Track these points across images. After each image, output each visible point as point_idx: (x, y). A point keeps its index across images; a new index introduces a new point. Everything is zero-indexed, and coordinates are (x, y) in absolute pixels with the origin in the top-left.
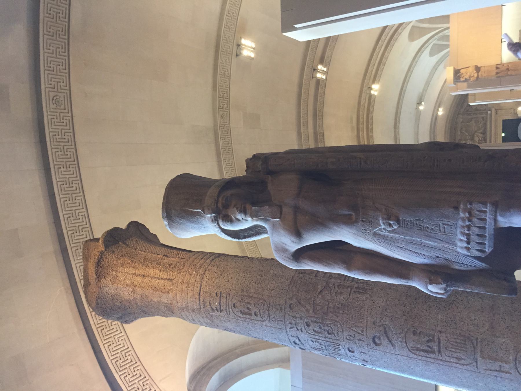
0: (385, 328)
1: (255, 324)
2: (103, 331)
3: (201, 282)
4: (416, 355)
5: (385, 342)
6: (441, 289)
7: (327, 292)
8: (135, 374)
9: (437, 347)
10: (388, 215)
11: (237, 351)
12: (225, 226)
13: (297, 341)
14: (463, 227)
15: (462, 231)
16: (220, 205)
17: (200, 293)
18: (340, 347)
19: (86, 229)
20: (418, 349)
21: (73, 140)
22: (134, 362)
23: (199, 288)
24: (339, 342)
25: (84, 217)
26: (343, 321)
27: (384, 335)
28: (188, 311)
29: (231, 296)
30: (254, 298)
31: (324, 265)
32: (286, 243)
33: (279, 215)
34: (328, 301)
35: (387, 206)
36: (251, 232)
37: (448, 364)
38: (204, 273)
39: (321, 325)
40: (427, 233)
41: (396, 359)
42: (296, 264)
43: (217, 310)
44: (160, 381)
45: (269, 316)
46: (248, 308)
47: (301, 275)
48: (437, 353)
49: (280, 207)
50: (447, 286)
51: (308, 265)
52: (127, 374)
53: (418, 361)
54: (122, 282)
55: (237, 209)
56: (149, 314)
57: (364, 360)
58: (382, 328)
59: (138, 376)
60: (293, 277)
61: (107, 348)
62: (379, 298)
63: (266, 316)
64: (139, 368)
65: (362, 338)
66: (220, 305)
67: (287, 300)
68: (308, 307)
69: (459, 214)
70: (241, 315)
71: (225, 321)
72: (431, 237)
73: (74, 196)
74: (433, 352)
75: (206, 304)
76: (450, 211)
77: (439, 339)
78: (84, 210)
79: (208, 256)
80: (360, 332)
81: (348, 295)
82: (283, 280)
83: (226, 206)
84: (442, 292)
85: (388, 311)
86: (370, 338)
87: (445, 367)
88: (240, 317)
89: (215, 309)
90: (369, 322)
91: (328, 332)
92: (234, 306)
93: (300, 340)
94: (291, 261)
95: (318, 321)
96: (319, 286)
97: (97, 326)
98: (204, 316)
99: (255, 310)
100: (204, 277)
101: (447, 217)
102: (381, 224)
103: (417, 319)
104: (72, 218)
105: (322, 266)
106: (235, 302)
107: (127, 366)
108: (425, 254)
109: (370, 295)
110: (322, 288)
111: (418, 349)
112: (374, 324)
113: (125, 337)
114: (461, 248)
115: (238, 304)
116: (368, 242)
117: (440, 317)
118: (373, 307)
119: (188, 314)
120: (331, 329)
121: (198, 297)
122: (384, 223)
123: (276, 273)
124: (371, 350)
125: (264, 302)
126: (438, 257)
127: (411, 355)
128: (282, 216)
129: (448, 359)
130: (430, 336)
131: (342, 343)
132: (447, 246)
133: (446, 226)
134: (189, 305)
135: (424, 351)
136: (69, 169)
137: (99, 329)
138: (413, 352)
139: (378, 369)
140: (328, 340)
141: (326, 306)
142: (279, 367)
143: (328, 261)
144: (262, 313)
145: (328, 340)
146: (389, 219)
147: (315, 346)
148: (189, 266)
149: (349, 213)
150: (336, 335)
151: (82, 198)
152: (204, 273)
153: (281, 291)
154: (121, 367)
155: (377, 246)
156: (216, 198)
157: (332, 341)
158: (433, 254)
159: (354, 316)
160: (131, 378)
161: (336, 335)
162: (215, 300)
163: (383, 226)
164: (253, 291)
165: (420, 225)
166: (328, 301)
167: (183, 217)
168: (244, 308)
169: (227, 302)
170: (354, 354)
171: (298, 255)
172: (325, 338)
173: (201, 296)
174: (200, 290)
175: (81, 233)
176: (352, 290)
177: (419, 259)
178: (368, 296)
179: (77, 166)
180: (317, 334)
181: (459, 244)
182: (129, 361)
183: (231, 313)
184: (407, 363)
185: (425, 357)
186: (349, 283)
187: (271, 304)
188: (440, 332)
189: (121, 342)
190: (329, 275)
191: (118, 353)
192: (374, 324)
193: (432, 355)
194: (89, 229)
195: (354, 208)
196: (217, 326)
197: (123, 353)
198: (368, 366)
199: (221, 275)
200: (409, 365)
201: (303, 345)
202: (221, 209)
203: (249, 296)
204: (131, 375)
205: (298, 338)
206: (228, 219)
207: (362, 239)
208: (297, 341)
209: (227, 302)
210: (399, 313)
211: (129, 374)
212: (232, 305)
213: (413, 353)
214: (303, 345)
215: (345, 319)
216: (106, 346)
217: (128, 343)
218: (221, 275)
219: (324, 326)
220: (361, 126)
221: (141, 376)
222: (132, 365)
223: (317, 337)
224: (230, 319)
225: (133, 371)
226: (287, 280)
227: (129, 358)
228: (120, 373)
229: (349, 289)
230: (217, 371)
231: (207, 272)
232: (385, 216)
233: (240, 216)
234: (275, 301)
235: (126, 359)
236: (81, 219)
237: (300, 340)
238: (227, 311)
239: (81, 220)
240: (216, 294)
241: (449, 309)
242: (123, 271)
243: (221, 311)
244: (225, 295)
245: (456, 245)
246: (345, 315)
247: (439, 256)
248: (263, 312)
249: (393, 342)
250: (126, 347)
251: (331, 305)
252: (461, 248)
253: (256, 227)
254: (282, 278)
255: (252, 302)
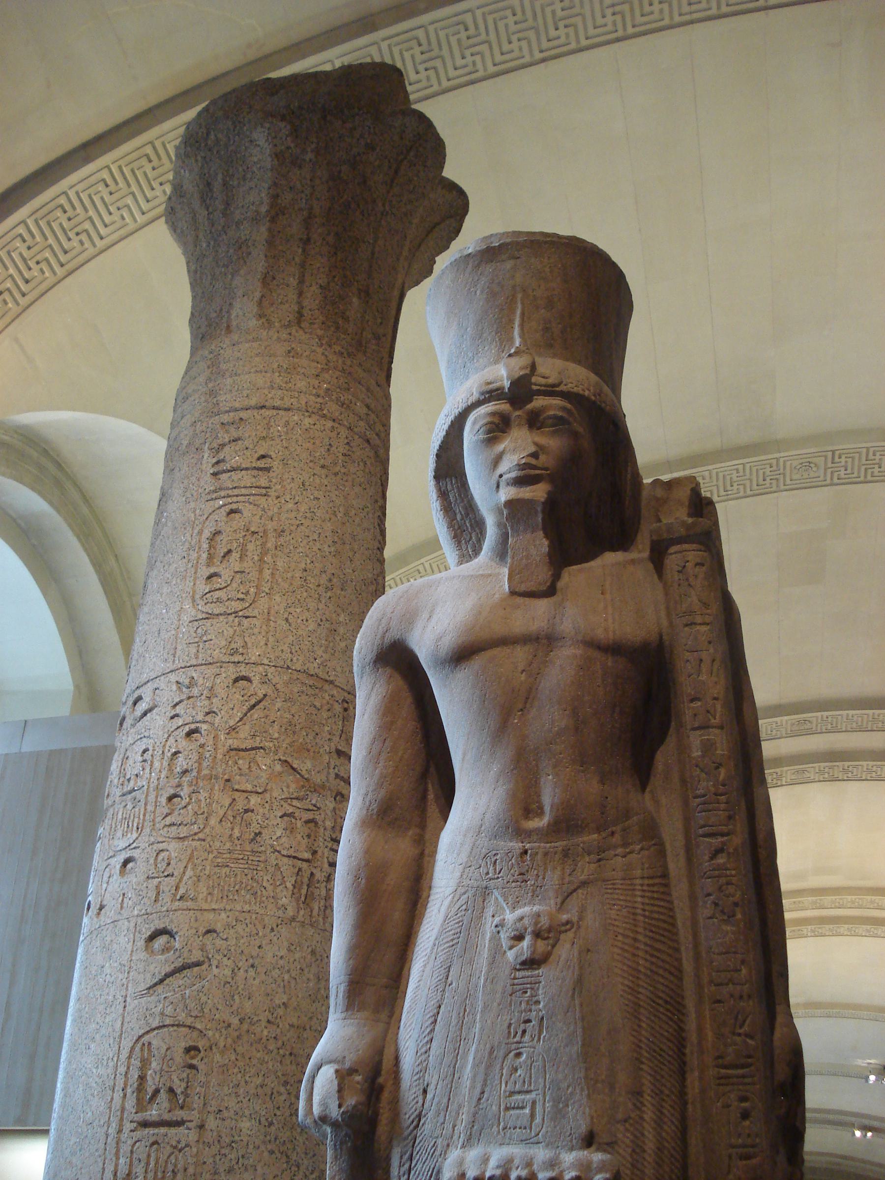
0: (198, 964)
1: (185, 578)
2: (144, 161)
3: (299, 409)
4: (130, 1057)
5: (160, 964)
6: (324, 1104)
7: (293, 786)
8: (32, 264)
9: (155, 1118)
10: (549, 930)
11: (112, 561)
12: (474, 423)
13: (142, 706)
14: (529, 1164)
15: (517, 1162)
16: (539, 402)
17: (263, 407)
18: (135, 835)
19: (434, 81)
20: (145, 1063)
21: (695, 16)
22: (63, 258)
23: (278, 403)
24: (147, 830)
25: (470, 68)
26: (209, 839)
27: (178, 964)
28: (210, 379)
29: (263, 499)
30: (261, 571)
31: (374, 740)
32: (435, 618)
33: (523, 588)
34: (265, 791)
35: (579, 927)
36: (459, 510)
37: (111, 1148)
38: (324, 416)
39: (194, 773)
40: (504, 1050)
41: (111, 998)
42: (370, 656)
43: (218, 463)
44: (16, 340)
45: (210, 616)
46: (229, 551)
47: (338, 708)
48: (139, 1117)
49: (550, 592)
50: (335, 1125)
51: (368, 697)
52: (30, 242)
53: (111, 1064)
54: (283, 182)
55: (535, 455)
56: (196, 272)
57: (101, 908)
58: (197, 956)
59: (27, 275)
60: (332, 682)
61: (99, 176)
62: (286, 944)
63: (209, 608)
64: (47, 274)
65: (166, 898)
66: (234, 469)
67: (261, 668)
68: (245, 731)
69: (572, 1149)
70: (207, 534)
71: (186, 489)
72: (489, 1067)
73: (531, 34)
74: (140, 1106)
75: (232, 429)
76: (578, 1120)
77: (179, 1124)
78: (491, 69)
79: (379, 427)
80: (181, 891)
81: (291, 852)
82: (320, 652)
83: (534, 421)
84: (316, 1110)
85: (252, 972)
86: (167, 920)
87: (103, 1141)
88: (200, 533)
89: (221, 456)
90: (211, 916)
91: (175, 796)
92: (232, 512)
93: (145, 714)
94: (378, 641)
95: (205, 764)
96: (309, 765)
97: (158, 144)
98: (199, 427)
99: (226, 575)
100: (315, 417)
101: (558, 1114)
102: (519, 912)
103: (233, 1058)
104: (463, 35)
105: (367, 740)
106: (246, 513)
107: (51, 241)
108: (432, 1052)
109: (293, 919)
110: (304, 773)
111: (145, 1063)
112: (209, 932)
113: (132, 226)
114: (461, 1162)
115: (238, 522)
116: (458, 874)
117: (245, 1124)
118: (259, 927)
119: (202, 379)
120: (183, 803)
121: (253, 402)
122: (521, 919)
123: (341, 630)
124: (132, 924)
125: (249, 599)
126: (425, 1092)
127: (127, 1044)
128: (520, 600)
129: (125, 1148)
130: (187, 1096)
131: (143, 843)
132: (465, 1117)
133: (527, 1111)
134: (229, 381)
135: (142, 1078)
136: (609, 12)
137: (149, 150)
138: (139, 1045)
139: (80, 951)
140: (152, 798)
141: (249, 787)
142: (77, 687)
143: (384, 756)
144: (217, 594)
145: (152, 798)
146: (537, 935)
147: (130, 761)
148: (343, 371)
149: (547, 809)
150: (168, 820)
151: (527, 59)
152: (324, 416)
153: (285, 648)
154: (49, 223)
155: (447, 903)
156: (562, 388)
157: (150, 808)
158: (432, 1078)
159: (225, 870)
160: (21, 255)
161: (168, 820)
162: (248, 453)
163: (510, 917)
164: (280, 564)
165: (524, 1032)
166: (265, 791)
167: (492, 295)
168: (230, 542)
169: (244, 491)
170: (116, 876)
171: (397, 659)
172: (157, 788)
173: (255, 412)
174: (274, 408)
175: (421, 68)
176: (305, 865)
177: (415, 1035)
178: (290, 912)
179: (620, 33)
180: (165, 764)
181: (473, 1154)
182: (66, 245)
183: (209, 507)
184: (103, 1031)
185: (126, 1084)
186: (321, 846)
187: (246, 622)
188: (201, 1127)
189: (116, 217)
190: (344, 792)
191: (86, 210)
192: (209, 932)
193: (131, 1103)
194: (436, 88)
195: (566, 824)
196: (169, 470)
197: (87, 225)
198: (86, 920)
199: (323, 467)
200: (98, 1037)
201: (133, 726)
202: (529, 407)
203: (264, 552)
204: (26, 254)
205: (150, 710)
206: (498, 428)
207: (463, 857)
208: (142, 706)
209: (244, 491)
210: (248, 1004)
211: (29, 248)
212: (234, 506)
213: (132, 1049)
214: (133, 726)
215: (218, 844)
216: (105, 174)
217: (115, 237)
218: (323, 467)
219: (190, 784)
220: (808, 900)
221: (27, 282)
222: (55, 255)
223: (157, 764)
224: (192, 505)
225: (38, 258)
226: (323, 665)
227: (75, 243)
228: (30, 222)
229: (307, 855)
230: (51, 503)
231: (329, 424)
232: (544, 922)
233: (508, 465)
234: (256, 631)
235: (71, 234)
236: (464, 62)
237: (145, 714)
238: (215, 491)
239: (459, 62)
240: (263, 457)
241: (272, 1152)
242: (317, 182)
243: (215, 474)
244: (263, 482)
245: (469, 1142)
246: (228, 845)
247: (429, 1096)
248: (219, 600)
249: (160, 989)
250: (103, 231)
251: (254, 800)
252: (461, 1162)
253: (479, 525)
254: (325, 652)
255: (247, 565)
